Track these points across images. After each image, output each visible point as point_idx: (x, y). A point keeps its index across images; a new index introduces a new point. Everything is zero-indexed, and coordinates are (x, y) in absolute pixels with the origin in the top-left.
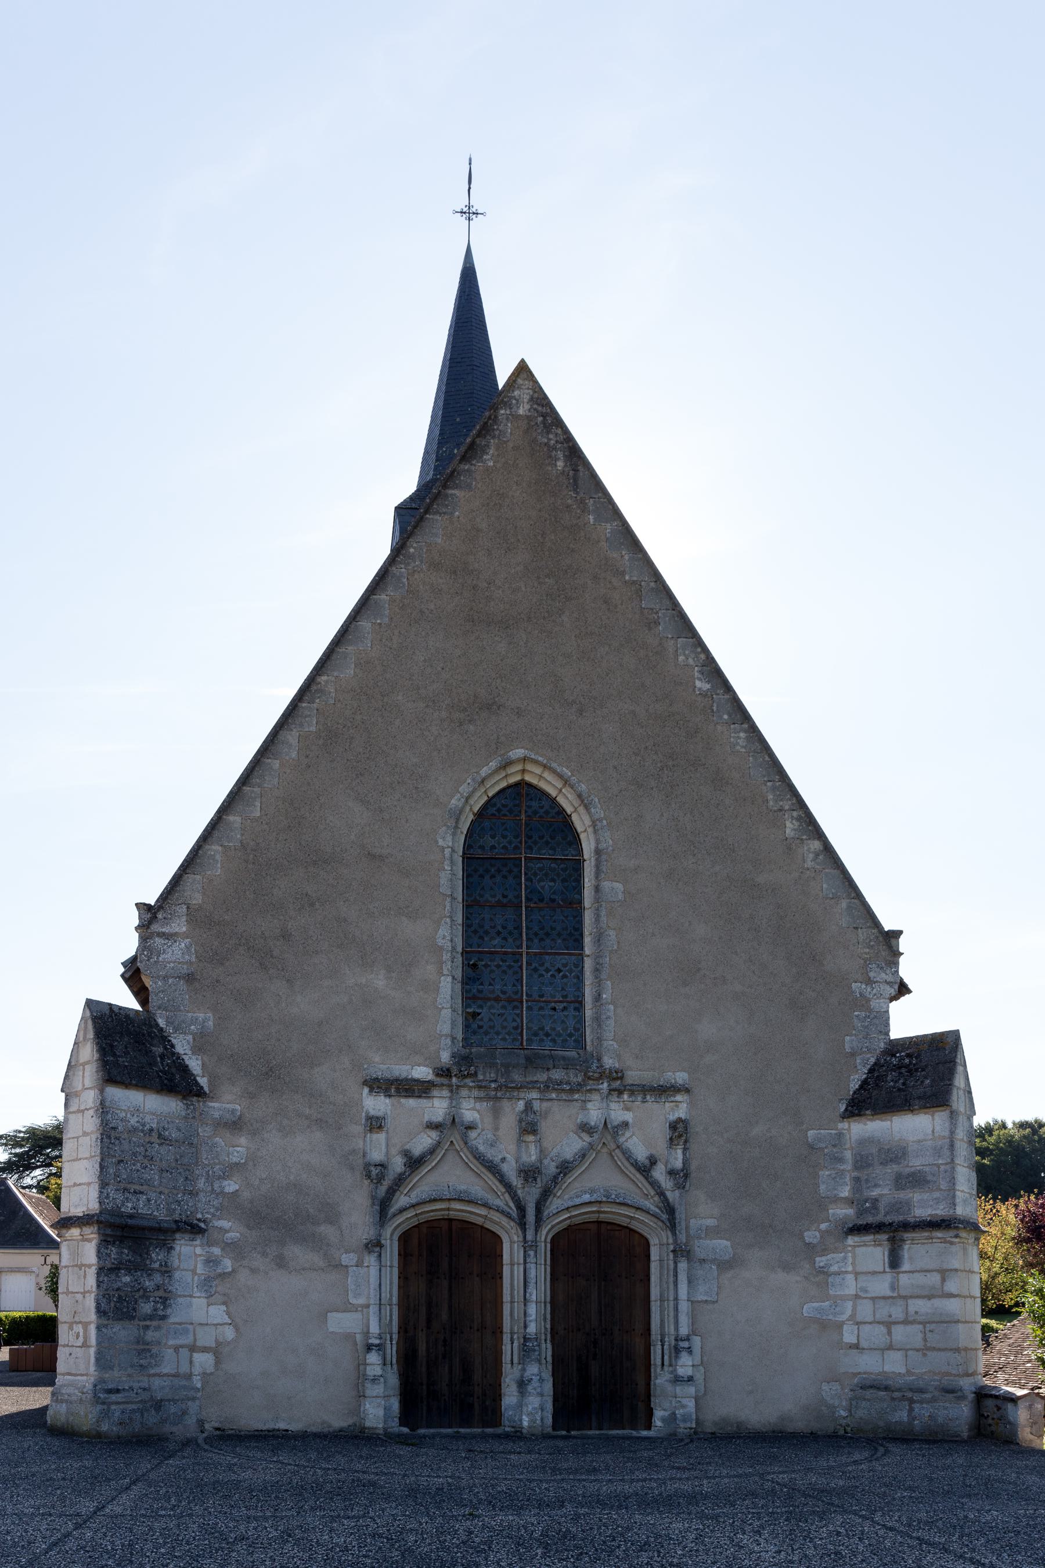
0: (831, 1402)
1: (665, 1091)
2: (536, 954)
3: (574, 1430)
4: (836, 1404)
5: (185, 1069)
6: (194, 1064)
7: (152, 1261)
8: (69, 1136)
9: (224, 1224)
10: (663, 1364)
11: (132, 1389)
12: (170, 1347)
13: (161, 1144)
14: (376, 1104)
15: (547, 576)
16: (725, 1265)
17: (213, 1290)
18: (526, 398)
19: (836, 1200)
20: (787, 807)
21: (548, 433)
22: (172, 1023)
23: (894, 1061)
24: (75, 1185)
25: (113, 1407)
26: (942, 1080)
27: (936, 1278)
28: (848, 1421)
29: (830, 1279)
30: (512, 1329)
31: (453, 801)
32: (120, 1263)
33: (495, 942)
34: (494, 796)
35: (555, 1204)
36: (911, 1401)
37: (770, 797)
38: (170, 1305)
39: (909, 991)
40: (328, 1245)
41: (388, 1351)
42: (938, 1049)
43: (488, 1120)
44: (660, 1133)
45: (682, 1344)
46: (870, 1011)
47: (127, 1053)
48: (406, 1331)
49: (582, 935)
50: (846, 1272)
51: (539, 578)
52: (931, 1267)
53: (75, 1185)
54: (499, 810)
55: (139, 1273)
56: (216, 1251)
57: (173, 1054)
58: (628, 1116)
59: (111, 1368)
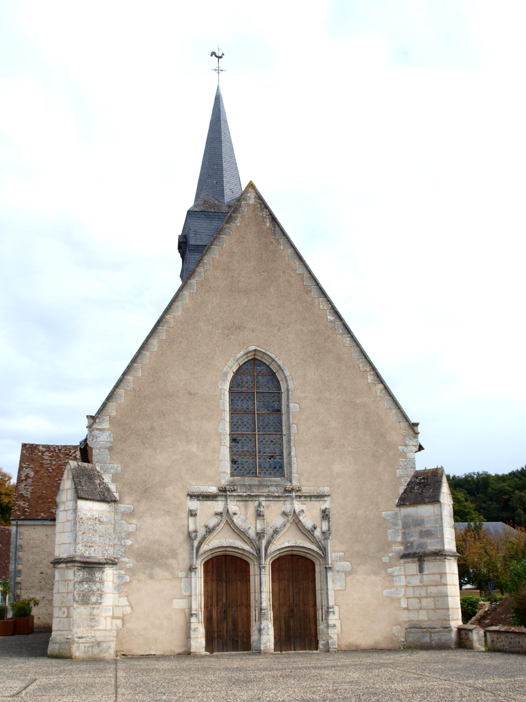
0: (397, 634)
1: (320, 497)
2: (262, 434)
3: (283, 651)
4: (399, 635)
5: (108, 490)
6: (113, 487)
7: (96, 578)
8: (60, 521)
9: (126, 560)
10: (322, 619)
11: (88, 636)
12: (103, 617)
13: (100, 524)
14: (194, 504)
15: (264, 272)
16: (347, 573)
17: (121, 590)
18: (253, 197)
19: (396, 542)
20: (368, 370)
21: (262, 211)
22: (103, 469)
23: (418, 481)
24: (62, 544)
25: (81, 645)
26: (437, 490)
27: (438, 577)
28: (405, 643)
29: (394, 579)
30: (255, 605)
31: (225, 369)
32: (84, 579)
33: (244, 429)
34: (242, 365)
35: (272, 548)
36: (431, 633)
37: (361, 365)
38: (103, 598)
39: (423, 449)
40: (173, 568)
41: (200, 617)
42: (435, 476)
43: (243, 510)
44: (317, 513)
45: (330, 610)
46: (407, 458)
47: (86, 484)
48: (207, 608)
49: (282, 425)
50: (401, 575)
51: (260, 272)
52: (435, 572)
53: (62, 544)
54: (244, 371)
55: (91, 583)
56: (123, 572)
57: (104, 483)
58: (304, 507)
59: (80, 627)
